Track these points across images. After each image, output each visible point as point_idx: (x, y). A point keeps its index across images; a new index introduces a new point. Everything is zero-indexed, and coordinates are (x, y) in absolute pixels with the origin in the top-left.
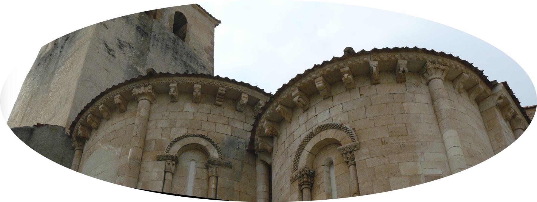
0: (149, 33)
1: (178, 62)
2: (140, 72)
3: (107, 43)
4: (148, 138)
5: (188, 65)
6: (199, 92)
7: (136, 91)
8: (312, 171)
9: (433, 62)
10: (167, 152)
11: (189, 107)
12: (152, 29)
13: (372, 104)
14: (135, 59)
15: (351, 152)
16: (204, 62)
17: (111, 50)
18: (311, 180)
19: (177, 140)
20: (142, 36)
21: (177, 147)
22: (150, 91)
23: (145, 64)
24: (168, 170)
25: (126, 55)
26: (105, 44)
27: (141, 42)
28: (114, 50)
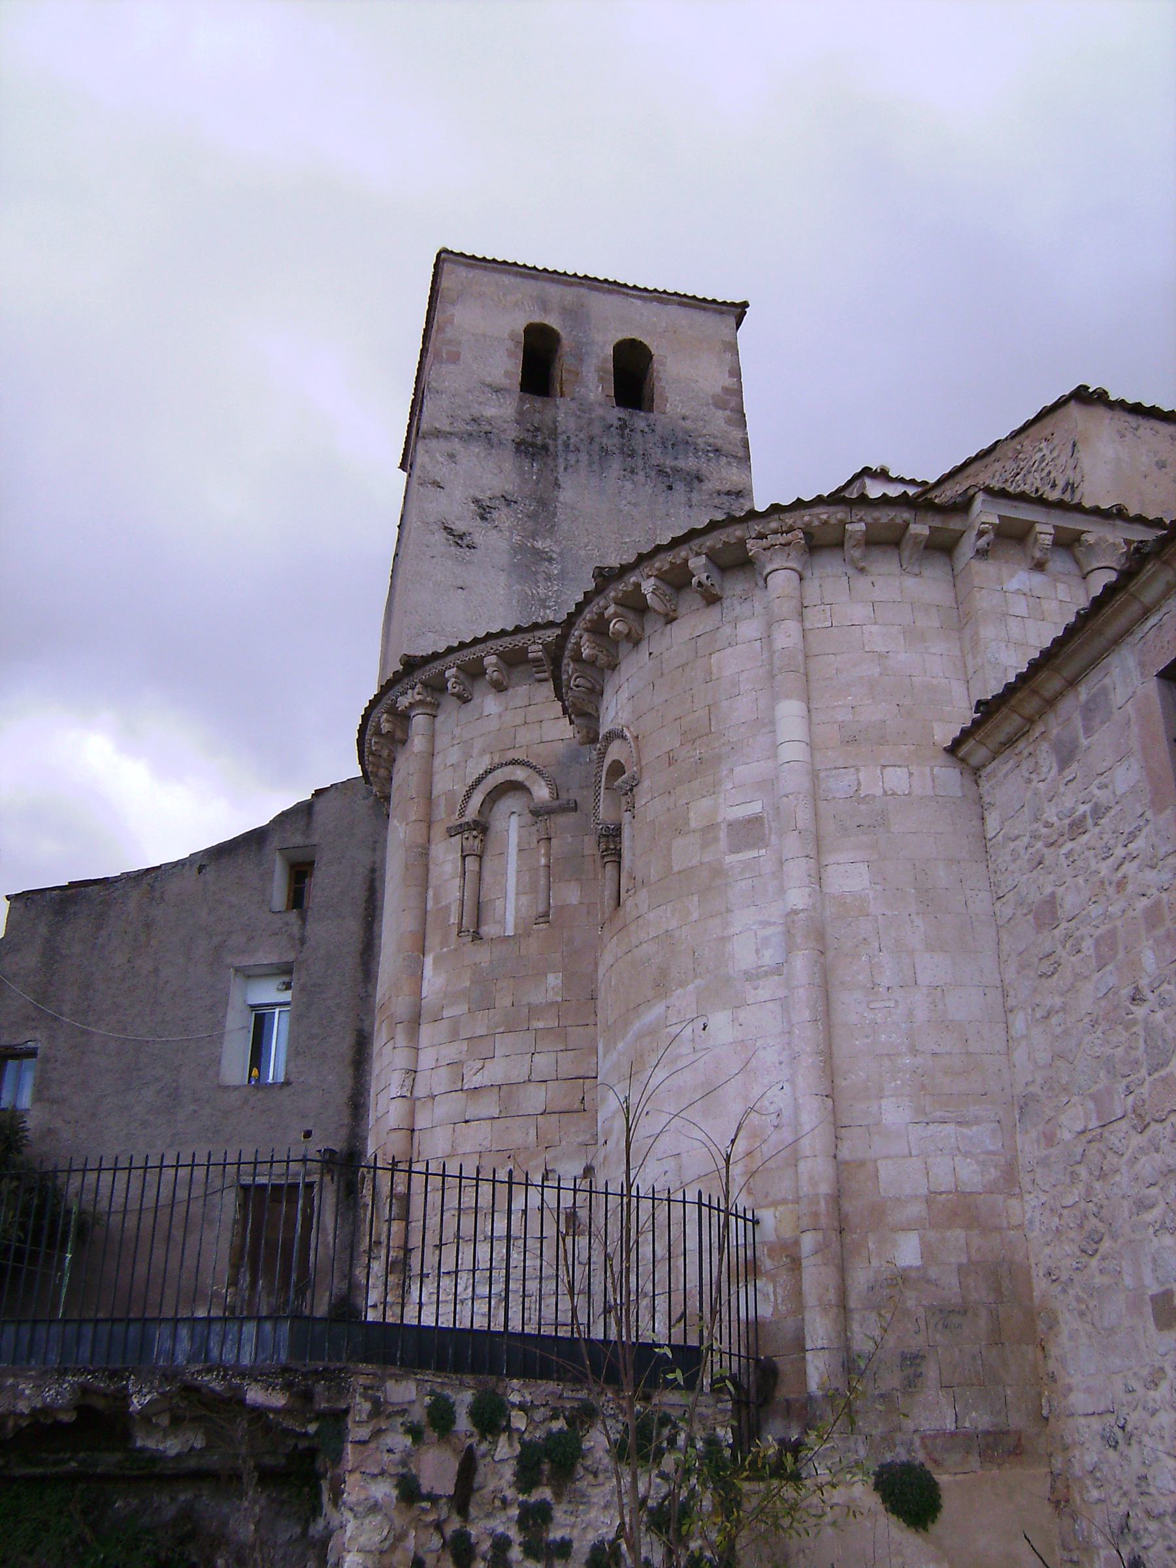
0: (551, 442)
1: (641, 477)
2: (546, 550)
3: (450, 522)
4: (435, 793)
5: (668, 470)
6: (495, 671)
7: (403, 702)
8: (613, 827)
9: (761, 536)
10: (462, 815)
11: (491, 704)
12: (556, 428)
13: (662, 673)
14: (526, 526)
15: (631, 790)
16: (715, 438)
17: (461, 537)
18: (614, 842)
19: (476, 785)
20: (533, 460)
21: (477, 798)
22: (418, 697)
23: (553, 526)
24: (468, 853)
25: (503, 529)
26: (446, 528)
27: (534, 477)
28: (470, 531)
